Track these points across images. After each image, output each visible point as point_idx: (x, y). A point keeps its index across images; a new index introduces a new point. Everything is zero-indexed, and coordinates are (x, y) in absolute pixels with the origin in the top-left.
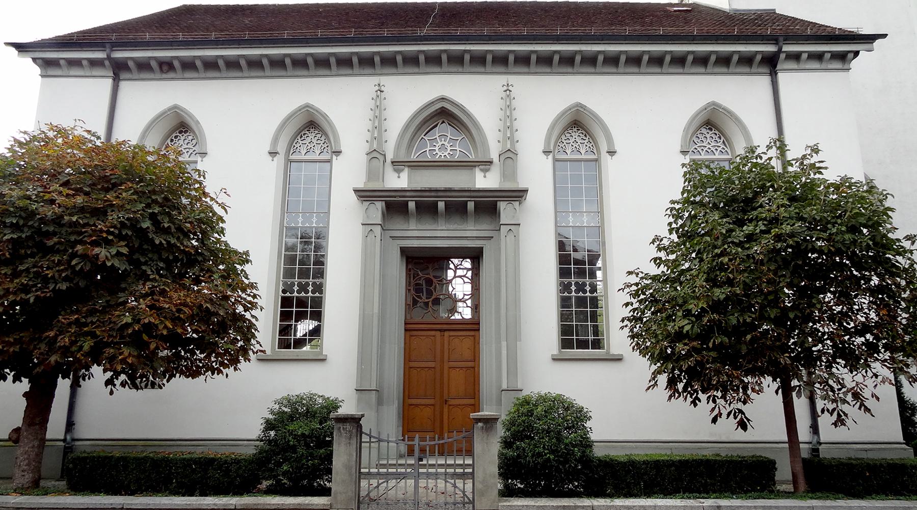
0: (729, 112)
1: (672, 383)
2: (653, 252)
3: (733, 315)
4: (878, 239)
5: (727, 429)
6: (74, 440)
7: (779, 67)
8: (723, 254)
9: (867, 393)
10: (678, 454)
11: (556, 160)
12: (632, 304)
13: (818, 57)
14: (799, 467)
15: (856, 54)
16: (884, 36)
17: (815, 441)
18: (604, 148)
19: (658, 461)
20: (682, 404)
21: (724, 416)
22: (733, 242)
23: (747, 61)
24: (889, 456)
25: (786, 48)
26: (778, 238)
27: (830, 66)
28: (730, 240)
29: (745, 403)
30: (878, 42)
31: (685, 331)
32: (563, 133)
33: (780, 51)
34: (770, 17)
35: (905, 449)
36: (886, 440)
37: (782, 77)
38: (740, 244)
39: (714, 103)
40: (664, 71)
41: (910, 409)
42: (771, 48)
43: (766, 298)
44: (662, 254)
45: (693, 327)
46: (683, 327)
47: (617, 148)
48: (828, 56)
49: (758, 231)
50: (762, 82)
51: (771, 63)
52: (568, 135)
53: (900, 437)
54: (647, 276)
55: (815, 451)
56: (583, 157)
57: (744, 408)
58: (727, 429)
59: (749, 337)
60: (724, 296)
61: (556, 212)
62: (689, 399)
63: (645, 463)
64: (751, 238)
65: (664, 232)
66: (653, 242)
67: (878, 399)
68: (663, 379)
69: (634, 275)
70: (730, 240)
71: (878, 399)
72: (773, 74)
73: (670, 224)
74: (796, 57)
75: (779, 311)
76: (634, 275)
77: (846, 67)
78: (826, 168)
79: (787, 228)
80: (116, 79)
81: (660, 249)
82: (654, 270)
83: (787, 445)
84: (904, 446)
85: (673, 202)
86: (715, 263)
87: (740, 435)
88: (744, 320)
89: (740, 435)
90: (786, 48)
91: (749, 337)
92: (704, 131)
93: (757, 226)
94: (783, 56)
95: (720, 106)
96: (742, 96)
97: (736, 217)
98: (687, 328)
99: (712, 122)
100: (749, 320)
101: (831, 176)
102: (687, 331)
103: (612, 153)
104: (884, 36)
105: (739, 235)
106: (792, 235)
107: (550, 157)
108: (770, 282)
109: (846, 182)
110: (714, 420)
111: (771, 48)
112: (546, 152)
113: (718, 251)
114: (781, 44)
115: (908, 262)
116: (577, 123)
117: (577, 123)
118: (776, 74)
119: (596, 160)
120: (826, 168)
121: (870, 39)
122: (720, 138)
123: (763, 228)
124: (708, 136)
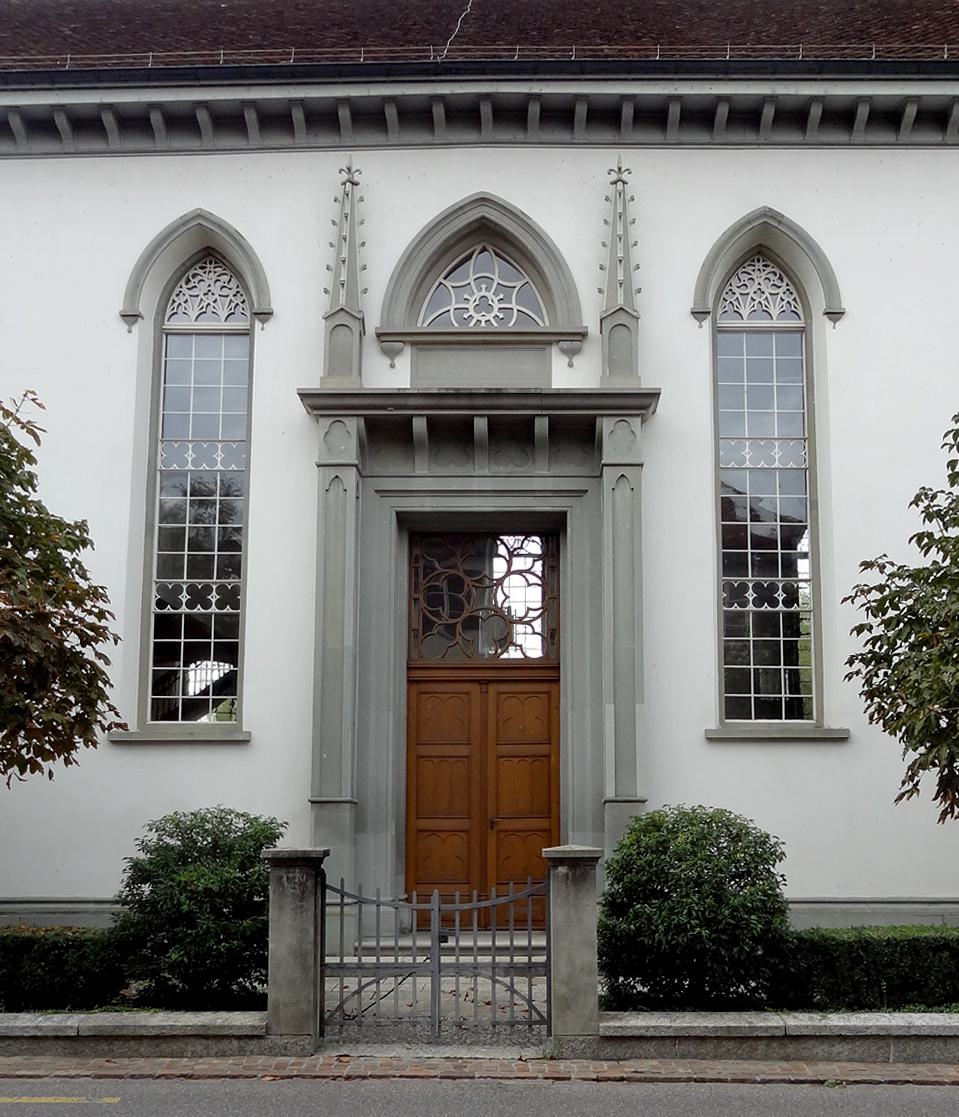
11: (717, 331)
12: (870, 629)
18: (819, 304)
32: (732, 272)
44: (935, 527)
47: (847, 302)
54: (902, 572)
68: (930, 779)
81: (929, 516)
103: (835, 315)
112: (699, 314)
117: (764, 248)
119: (802, 331)
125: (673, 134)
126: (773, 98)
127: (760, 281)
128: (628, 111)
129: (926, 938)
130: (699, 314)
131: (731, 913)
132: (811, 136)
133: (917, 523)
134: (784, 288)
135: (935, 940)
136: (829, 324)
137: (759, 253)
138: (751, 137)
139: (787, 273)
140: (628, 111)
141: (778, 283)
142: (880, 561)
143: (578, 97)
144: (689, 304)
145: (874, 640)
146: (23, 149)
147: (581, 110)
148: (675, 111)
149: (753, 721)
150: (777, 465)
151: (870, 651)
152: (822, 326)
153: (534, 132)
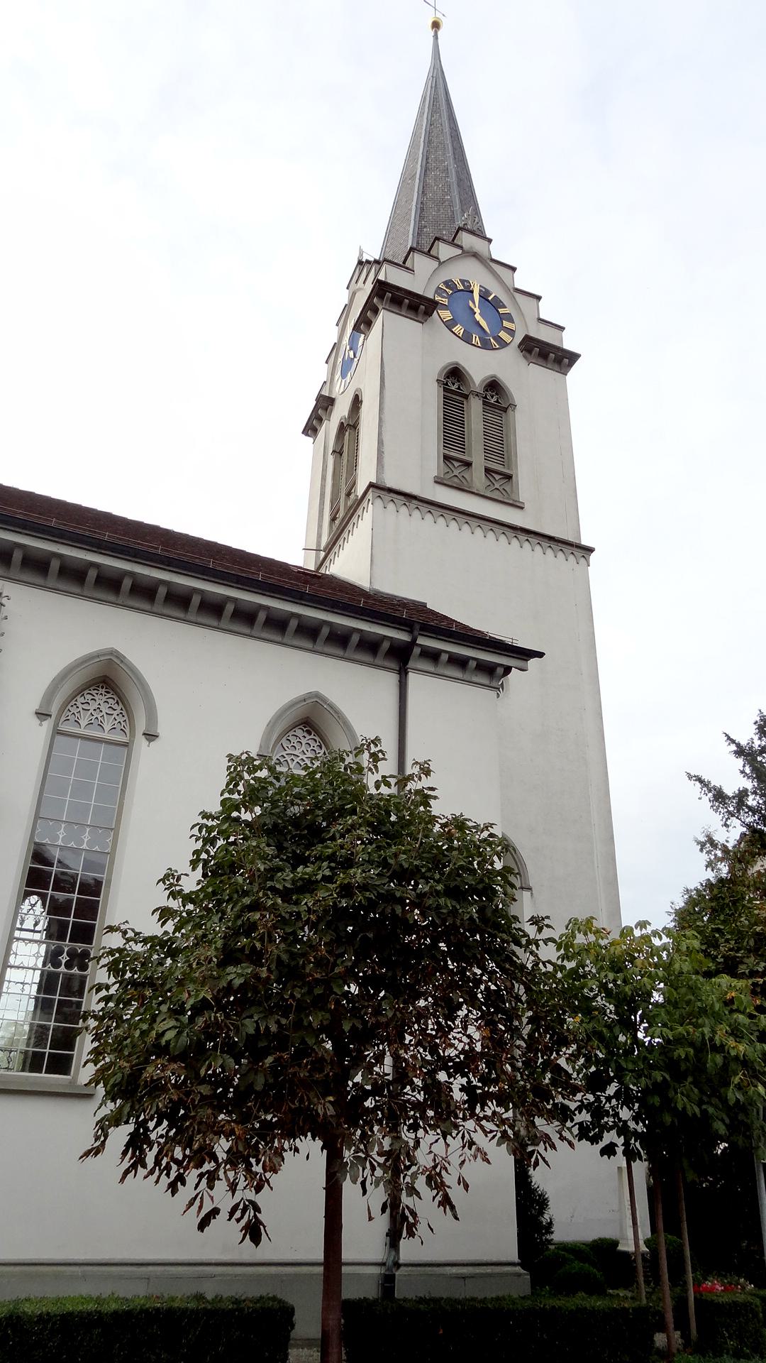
0: (337, 712)
1: (137, 1143)
2: (161, 898)
3: (251, 1017)
4: (489, 914)
5: (225, 1240)
6: (268, 1181)
7: (411, 664)
8: (255, 906)
9: (450, 1179)
10: (133, 1292)
11: (57, 732)
12: (108, 987)
13: (460, 663)
14: (336, 1320)
15: (508, 670)
16: (540, 655)
17: (390, 1263)
18: (141, 726)
19: (70, 1314)
20: (147, 1189)
21: (224, 1214)
22: (273, 889)
23: (370, 646)
24: (488, 1292)
25: (421, 641)
26: (346, 890)
27: (475, 679)
28: (269, 884)
29: (258, 1189)
30: (533, 662)
31: (163, 1043)
32: (80, 692)
33: (413, 643)
34: (421, 608)
35: (519, 1275)
36: (495, 1259)
37: (412, 677)
38: (286, 895)
39: (317, 695)
40: (254, 633)
41: (538, 1202)
42: (403, 636)
43: (310, 992)
44: (175, 904)
45: (179, 1033)
46: (164, 1032)
47: (161, 730)
48: (473, 664)
49: (319, 877)
50: (388, 680)
51: (400, 658)
52: (90, 697)
53: (513, 1255)
54: (137, 937)
55: (388, 1281)
56: (106, 736)
57: (260, 1199)
58: (225, 1240)
59: (270, 1059)
60: (242, 980)
61: (37, 817)
62: (165, 1181)
63: (44, 1319)
64: (308, 886)
65: (183, 866)
66: (163, 880)
67: (466, 1187)
68: (120, 1135)
69: (118, 935)
70: (269, 884)
71: (466, 1187)
72: (403, 673)
73: (197, 852)
74: (433, 656)
75: (328, 1016)
76: (118, 935)
77: (494, 684)
78: (435, 798)
79: (357, 875)
80: (403, 673)
81: (173, 895)
82: (153, 928)
83: (321, 1269)
84: (518, 1269)
85: (205, 815)
86: (239, 922)
87: (248, 1252)
88: (267, 1028)
89: (248, 1252)
90: (422, 641)
91: (270, 1059)
92: (299, 733)
93: (320, 868)
94: (417, 651)
95: (325, 700)
96: (362, 698)
97: (294, 852)
98: (170, 1035)
99: (310, 719)
100: (274, 1028)
101: (442, 808)
102: (168, 1042)
103: (151, 737)
104: (540, 655)
105: (286, 878)
106: (364, 887)
107: (48, 725)
108: (320, 963)
109: (459, 824)
110: (202, 1225)
111: (403, 636)
112: (42, 715)
113: (247, 901)
114: (416, 633)
115: (532, 958)
116: (106, 680)
117: (106, 680)
118: (406, 673)
119: (126, 745)
120: (435, 798)
121: (527, 655)
122: (320, 747)
123: (327, 873)
124: (304, 741)
125: (225, 623)
126: (235, 600)
127: (100, 702)
128: (262, 616)
129: (80, 1312)
130: (42, 715)
131: (645, 1092)
132: (349, 653)
133: (161, 898)
134: (118, 711)
135: (89, 1314)
136: (144, 742)
137: (104, 682)
138: (112, 598)
139: (121, 699)
140: (196, 600)
141: (115, 707)
142: (123, 927)
143: (261, 607)
144: (35, 706)
145: (107, 999)
146: (192, 618)
147: (196, 600)
148: (230, 608)
149: (43, 1075)
150: (84, 846)
151: (103, 1009)
152: (141, 742)
153: (51, 582)
